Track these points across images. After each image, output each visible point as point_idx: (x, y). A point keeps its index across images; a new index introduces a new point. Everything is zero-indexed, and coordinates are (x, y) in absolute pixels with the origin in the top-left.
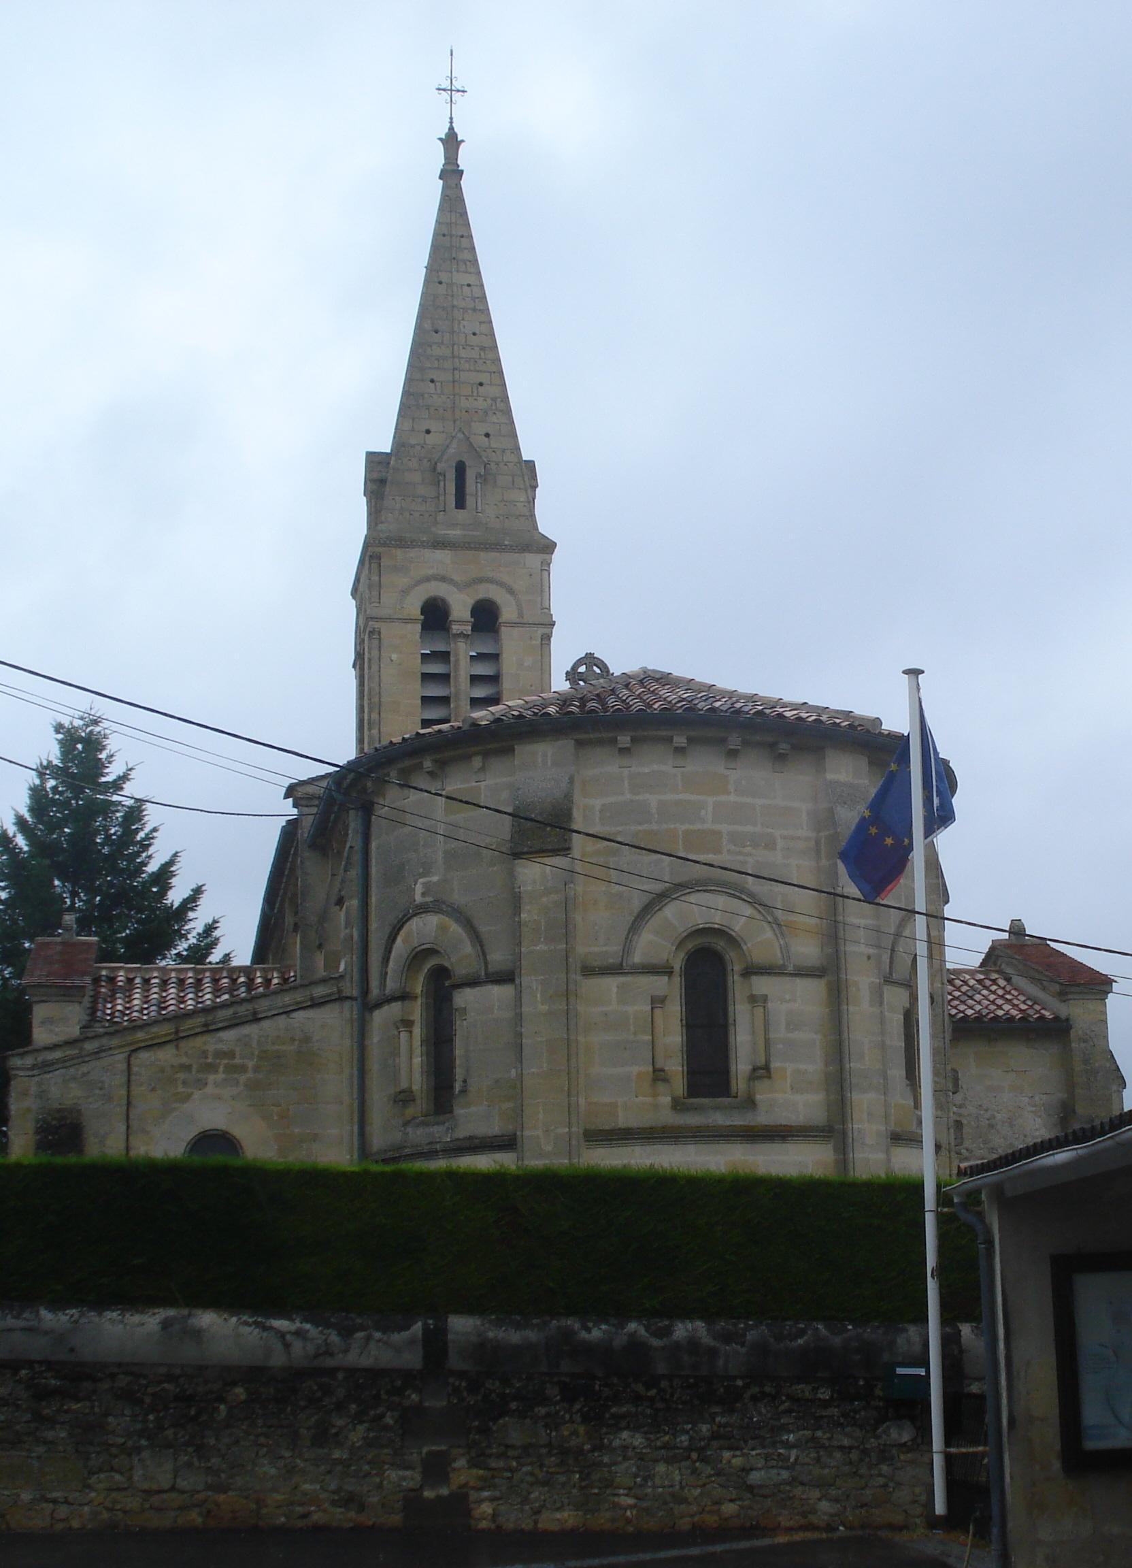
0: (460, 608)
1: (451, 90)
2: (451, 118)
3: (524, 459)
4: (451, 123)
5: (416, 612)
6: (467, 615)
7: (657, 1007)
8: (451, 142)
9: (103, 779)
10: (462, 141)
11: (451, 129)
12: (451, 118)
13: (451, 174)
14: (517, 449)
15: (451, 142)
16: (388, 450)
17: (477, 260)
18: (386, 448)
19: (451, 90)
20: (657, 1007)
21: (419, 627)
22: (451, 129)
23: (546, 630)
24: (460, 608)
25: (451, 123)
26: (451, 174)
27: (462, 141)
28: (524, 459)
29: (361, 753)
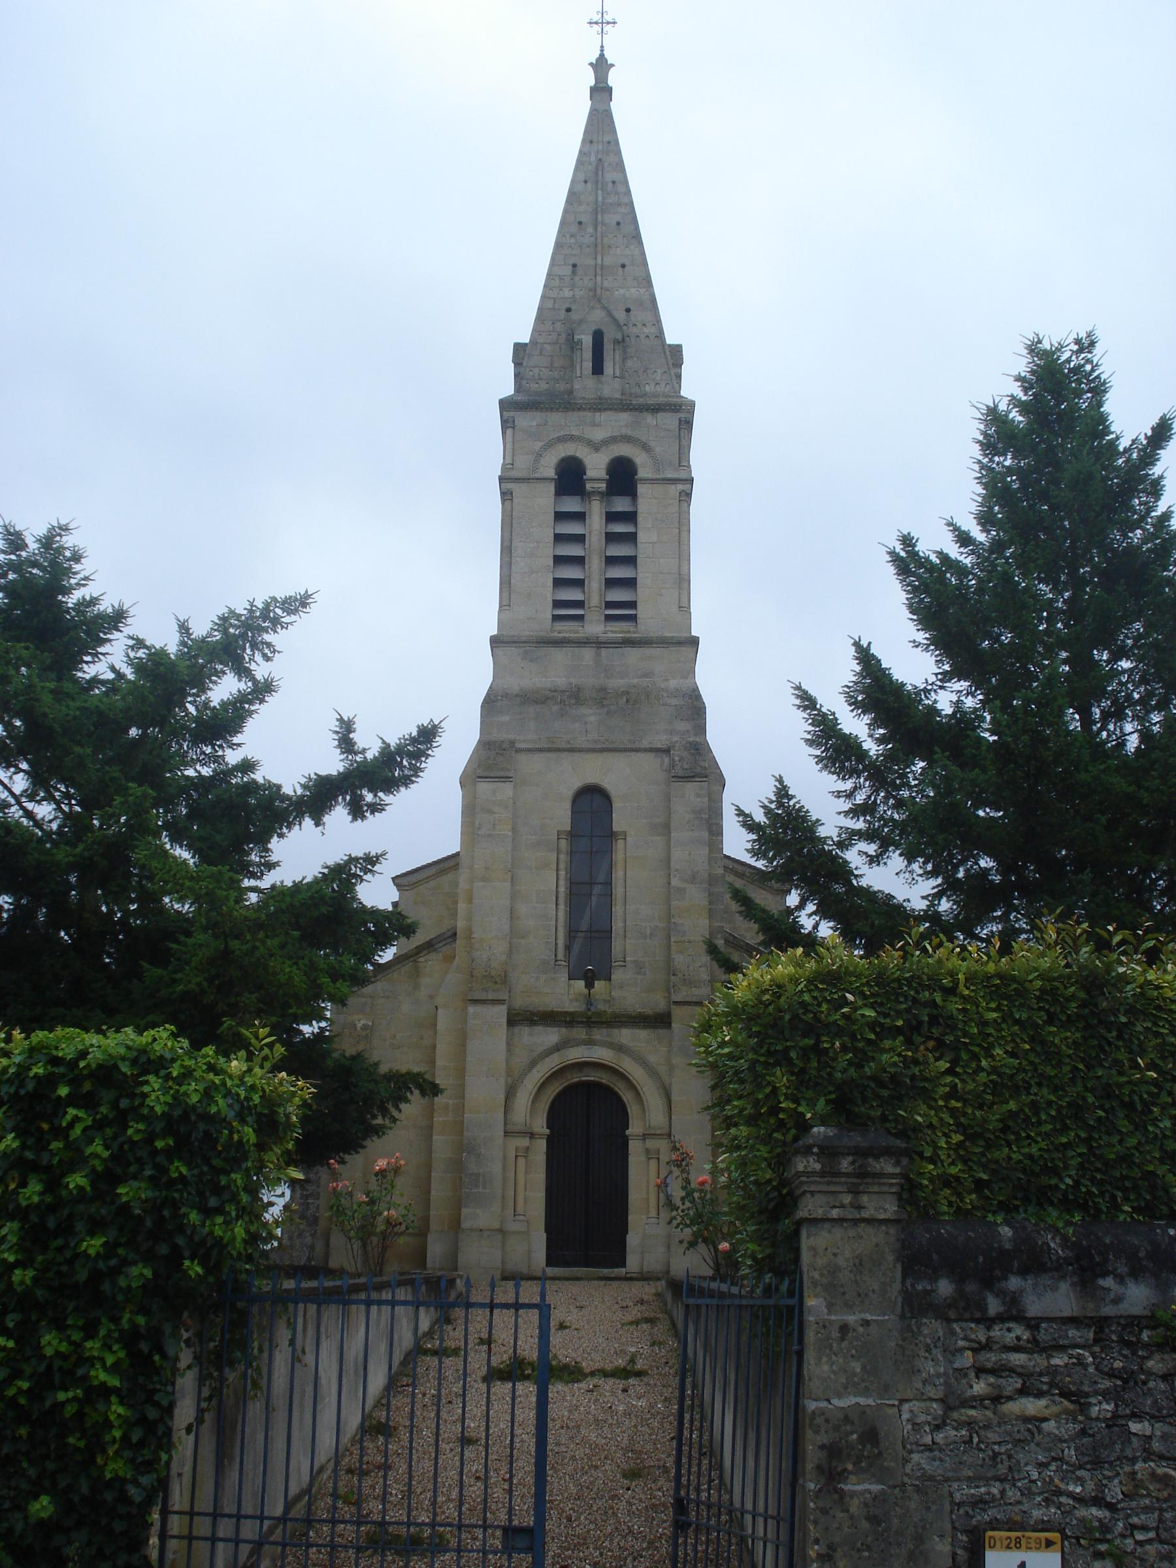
0: (596, 467)
1: (602, 23)
2: (602, 47)
3: (668, 342)
4: (602, 51)
5: (551, 473)
6: (603, 474)
7: (812, 1193)
8: (601, 66)
9: (80, 674)
10: (612, 65)
11: (602, 56)
12: (602, 47)
13: (601, 91)
14: (660, 335)
15: (601, 66)
16: (527, 341)
17: (630, 191)
18: (527, 341)
19: (602, 23)
20: (812, 1193)
21: (551, 488)
22: (602, 56)
23: (686, 487)
24: (596, 467)
25: (602, 51)
26: (601, 91)
27: (612, 65)
28: (668, 342)
29: (1084, 1404)
